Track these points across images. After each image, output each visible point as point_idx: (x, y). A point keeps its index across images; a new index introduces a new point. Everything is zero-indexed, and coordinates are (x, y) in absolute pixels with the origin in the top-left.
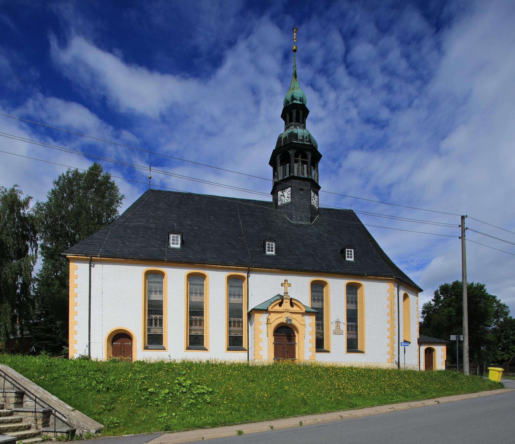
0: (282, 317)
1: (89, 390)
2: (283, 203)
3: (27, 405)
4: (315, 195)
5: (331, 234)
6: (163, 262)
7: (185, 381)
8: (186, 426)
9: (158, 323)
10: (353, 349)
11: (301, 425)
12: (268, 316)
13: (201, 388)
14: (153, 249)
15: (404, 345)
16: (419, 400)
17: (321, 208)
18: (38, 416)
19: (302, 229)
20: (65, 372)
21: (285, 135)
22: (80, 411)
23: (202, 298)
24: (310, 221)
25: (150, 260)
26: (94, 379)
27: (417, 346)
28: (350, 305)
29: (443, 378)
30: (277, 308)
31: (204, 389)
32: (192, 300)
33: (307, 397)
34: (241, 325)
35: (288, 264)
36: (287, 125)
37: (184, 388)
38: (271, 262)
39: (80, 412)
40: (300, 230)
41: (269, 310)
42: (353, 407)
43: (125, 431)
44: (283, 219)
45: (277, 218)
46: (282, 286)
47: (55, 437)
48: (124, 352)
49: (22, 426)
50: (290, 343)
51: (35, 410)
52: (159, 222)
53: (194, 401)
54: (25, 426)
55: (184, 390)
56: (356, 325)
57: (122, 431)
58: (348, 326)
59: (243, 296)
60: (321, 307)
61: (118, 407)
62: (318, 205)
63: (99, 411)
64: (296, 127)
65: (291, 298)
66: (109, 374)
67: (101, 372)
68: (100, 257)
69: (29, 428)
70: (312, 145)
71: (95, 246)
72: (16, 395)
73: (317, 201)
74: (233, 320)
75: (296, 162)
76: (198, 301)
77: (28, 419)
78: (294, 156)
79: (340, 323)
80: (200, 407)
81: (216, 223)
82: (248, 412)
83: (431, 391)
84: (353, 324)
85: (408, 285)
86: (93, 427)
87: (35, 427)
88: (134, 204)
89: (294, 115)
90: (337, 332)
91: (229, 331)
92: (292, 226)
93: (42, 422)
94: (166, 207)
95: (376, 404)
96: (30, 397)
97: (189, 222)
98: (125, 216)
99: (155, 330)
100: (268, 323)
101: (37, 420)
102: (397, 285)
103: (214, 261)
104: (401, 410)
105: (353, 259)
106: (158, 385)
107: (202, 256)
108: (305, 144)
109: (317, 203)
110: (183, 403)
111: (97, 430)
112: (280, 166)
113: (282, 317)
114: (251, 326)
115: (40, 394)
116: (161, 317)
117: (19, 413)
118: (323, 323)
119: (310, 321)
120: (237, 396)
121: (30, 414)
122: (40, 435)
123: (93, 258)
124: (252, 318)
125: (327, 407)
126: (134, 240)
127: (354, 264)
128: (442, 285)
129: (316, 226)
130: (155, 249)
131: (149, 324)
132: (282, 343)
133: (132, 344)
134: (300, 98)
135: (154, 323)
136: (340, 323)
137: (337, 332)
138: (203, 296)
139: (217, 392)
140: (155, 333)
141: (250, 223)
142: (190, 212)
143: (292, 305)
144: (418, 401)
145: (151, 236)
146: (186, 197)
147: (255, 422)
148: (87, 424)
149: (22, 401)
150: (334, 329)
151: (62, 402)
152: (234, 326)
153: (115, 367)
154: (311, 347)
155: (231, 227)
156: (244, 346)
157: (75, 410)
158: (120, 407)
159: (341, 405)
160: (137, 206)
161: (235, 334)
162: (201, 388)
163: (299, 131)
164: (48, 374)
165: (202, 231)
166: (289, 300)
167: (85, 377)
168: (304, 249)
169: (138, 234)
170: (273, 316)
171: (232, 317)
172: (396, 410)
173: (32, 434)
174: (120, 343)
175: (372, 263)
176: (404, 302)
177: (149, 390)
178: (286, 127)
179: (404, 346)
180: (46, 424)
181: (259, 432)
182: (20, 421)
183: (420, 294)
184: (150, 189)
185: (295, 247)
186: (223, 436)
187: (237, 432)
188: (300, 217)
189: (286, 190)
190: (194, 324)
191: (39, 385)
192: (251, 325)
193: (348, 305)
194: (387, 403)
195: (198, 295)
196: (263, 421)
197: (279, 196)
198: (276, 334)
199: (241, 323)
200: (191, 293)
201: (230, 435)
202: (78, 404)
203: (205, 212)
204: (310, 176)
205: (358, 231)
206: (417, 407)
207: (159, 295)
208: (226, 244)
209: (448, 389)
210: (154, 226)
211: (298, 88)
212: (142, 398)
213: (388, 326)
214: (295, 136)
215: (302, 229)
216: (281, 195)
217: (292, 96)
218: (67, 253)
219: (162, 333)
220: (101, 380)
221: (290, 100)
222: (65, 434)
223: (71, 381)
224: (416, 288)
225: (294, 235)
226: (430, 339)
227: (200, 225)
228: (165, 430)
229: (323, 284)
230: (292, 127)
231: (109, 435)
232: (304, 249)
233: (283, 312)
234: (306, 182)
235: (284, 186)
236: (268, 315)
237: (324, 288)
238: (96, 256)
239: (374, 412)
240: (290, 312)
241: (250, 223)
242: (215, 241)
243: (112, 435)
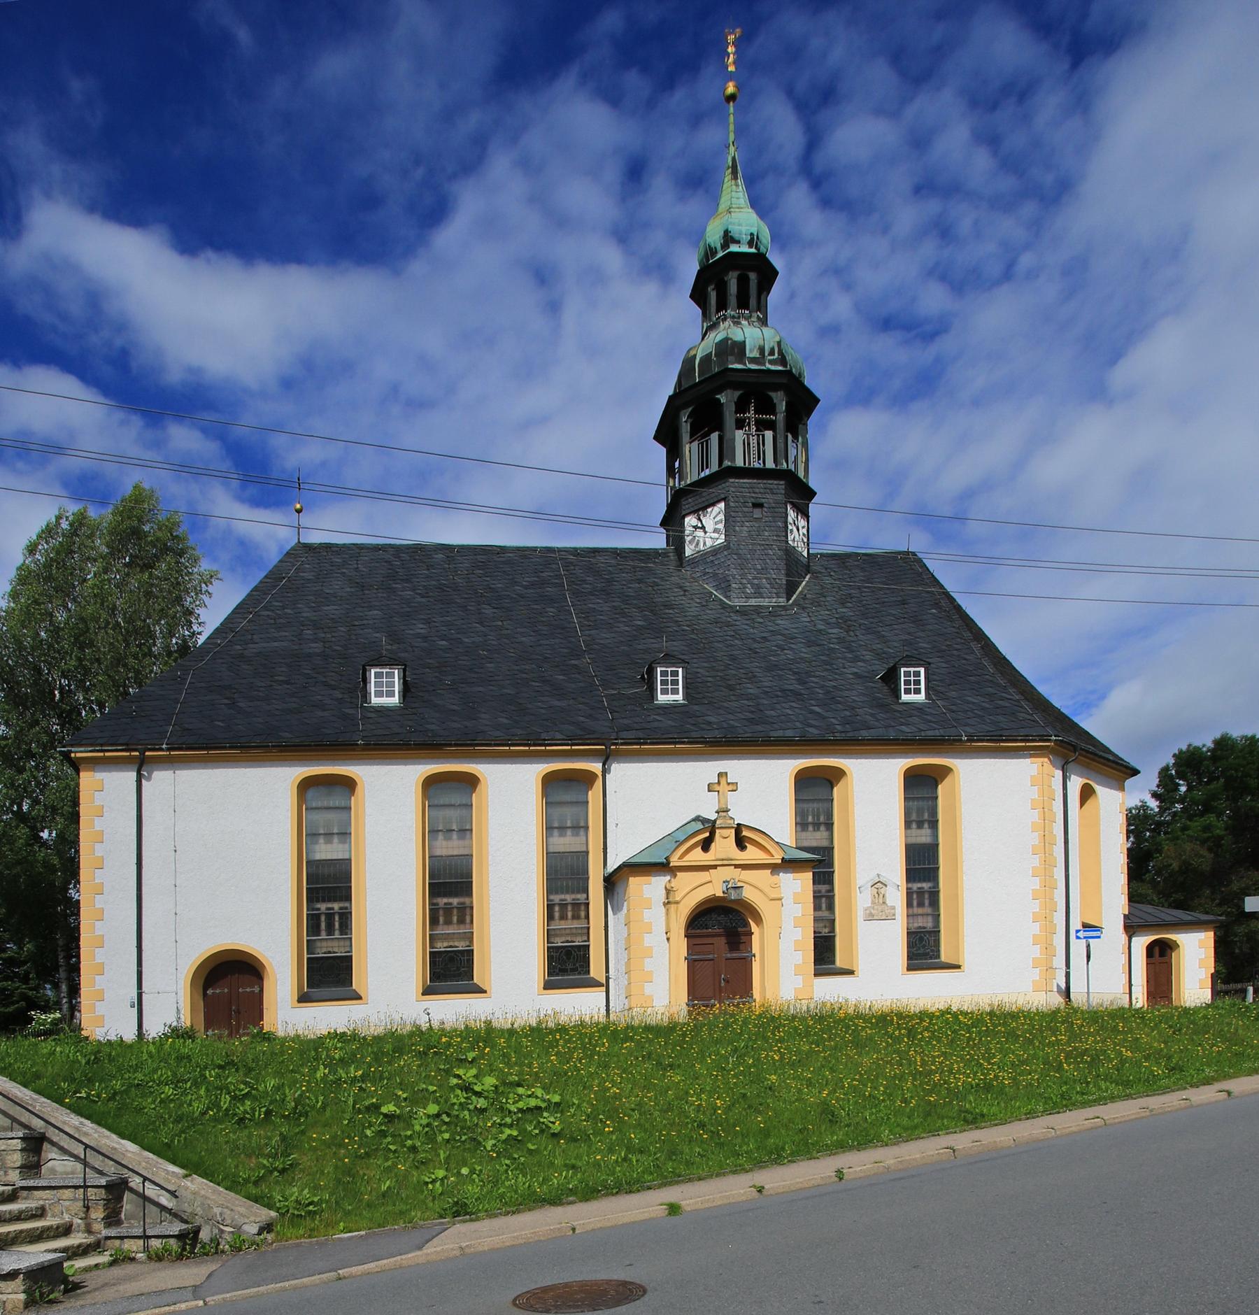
0: (711, 882)
1: (216, 1120)
2: (702, 548)
3: (53, 1171)
4: (799, 518)
5: (852, 629)
6: (354, 750)
7: (477, 1079)
8: (511, 1201)
9: (337, 925)
10: (926, 959)
11: (841, 1179)
12: (669, 881)
13: (529, 1096)
14: (320, 713)
15: (1085, 938)
16: (1165, 1090)
17: (816, 555)
18: (93, 1198)
19: (761, 620)
20: (140, 1076)
21: (703, 349)
22: (203, 1178)
23: (467, 842)
24: (784, 595)
25: (315, 745)
26: (224, 1088)
27: (1123, 938)
28: (914, 831)
29: (1229, 1024)
30: (698, 856)
31: (537, 1097)
32: (438, 852)
33: (838, 1100)
34: (583, 914)
35: (725, 725)
36: (710, 320)
37: (479, 1097)
38: (673, 724)
39: (205, 1181)
40: (756, 625)
41: (671, 864)
42: (975, 1123)
43: (342, 1224)
44: (702, 596)
45: (682, 593)
46: (709, 791)
47: (144, 1252)
48: (239, 1013)
49: (52, 1226)
50: (735, 955)
51: (85, 1181)
52: (333, 637)
53: (515, 1133)
54: (58, 1227)
55: (482, 1103)
56: (934, 888)
57: (331, 1225)
58: (909, 893)
59: (590, 829)
60: (825, 843)
61: (306, 1161)
62: (808, 545)
63: (256, 1174)
64: (737, 323)
65: (738, 824)
66: (260, 1073)
67: (237, 1070)
68: (168, 749)
69: (66, 1230)
70: (790, 372)
71: (152, 721)
72: (24, 1146)
73: (804, 534)
74: (561, 900)
75: (740, 424)
76: (455, 853)
77: (65, 1209)
78: (734, 409)
79: (886, 886)
80: (533, 1148)
81: (500, 623)
82: (674, 1153)
83: (1197, 1064)
84: (926, 886)
85: (1097, 758)
86: (252, 1219)
87: (83, 1226)
88: (255, 589)
89: (733, 287)
90: (879, 913)
91: (550, 933)
92: (731, 614)
93: (104, 1212)
94: (348, 589)
95: (1041, 1109)
96: (63, 1150)
97: (421, 628)
98: (231, 626)
99: (329, 946)
100: (669, 903)
101: (88, 1208)
102: (1060, 762)
103: (502, 734)
104: (1120, 1122)
105: (921, 697)
106: (405, 1095)
107: (465, 723)
108: (769, 371)
109: (805, 540)
110: (484, 1140)
111: (261, 1224)
112: (691, 443)
113: (711, 882)
114: (614, 914)
115: (90, 1137)
116: (346, 908)
117: (36, 1192)
118: (832, 890)
119: (799, 885)
120: (633, 1110)
121: (68, 1193)
122: (99, 1248)
123: (147, 753)
124: (619, 889)
125: (898, 1125)
126: (261, 694)
127: (927, 709)
128: (1181, 752)
129: (804, 608)
130: (326, 714)
131: (310, 930)
132: (711, 956)
133: (262, 990)
134: (749, 238)
135: (323, 925)
136: (886, 886)
137: (879, 913)
138: (468, 836)
139: (574, 1104)
140: (330, 952)
141: (601, 617)
142: (423, 600)
143: (741, 843)
144: (1164, 1093)
145: (313, 678)
146: (408, 558)
147: (700, 1179)
148: (232, 1210)
149: (39, 1161)
150: (865, 906)
151: (151, 1155)
152: (563, 917)
153: (273, 1053)
154: (801, 962)
155: (545, 633)
156: (592, 974)
157: (190, 1175)
158: (311, 1159)
159: (938, 1118)
160: (265, 594)
161: (568, 942)
162: (529, 1096)
163: (750, 334)
164: (97, 1084)
165: (459, 650)
166: (733, 831)
167: (196, 1084)
168: (771, 679)
169: (272, 677)
170: (684, 882)
171: (557, 893)
172: (1107, 1122)
173: (79, 1246)
174: (226, 990)
175: (984, 704)
176: (1081, 807)
177: (384, 1110)
178: (705, 325)
179: (1085, 940)
180: (112, 1218)
181: (725, 1205)
182: (40, 1213)
183: (1129, 782)
184: (299, 542)
185: (743, 676)
186: (626, 1220)
187: (665, 1207)
188: (752, 585)
189: (709, 510)
190: (441, 919)
191: (82, 1115)
192: (616, 910)
193: (909, 831)
194: (1074, 1105)
195: (455, 836)
196: (724, 1174)
197: (688, 530)
198: (693, 931)
199: (583, 907)
200: (434, 832)
201: (646, 1216)
202: (195, 1158)
203: (466, 596)
204: (785, 464)
205: (934, 611)
206: (1169, 1112)
207: (341, 846)
208: (533, 683)
209: (1249, 1055)
210: (316, 647)
211: (742, 206)
212: (368, 1132)
213: (1036, 883)
214: (736, 350)
215: (761, 620)
216: (696, 527)
217: (726, 233)
218: (72, 746)
219: (349, 952)
220: (243, 1090)
222: (172, 1241)
223: (161, 1099)
224: (1119, 767)
225: (737, 639)
226: (1163, 916)
227: (452, 634)
228: (454, 1213)
229: (832, 777)
230: (727, 323)
231: (297, 1238)
232: (771, 679)
233: (715, 867)
234: (770, 482)
235: (703, 499)
236: (668, 878)
237: (835, 789)
238: (157, 747)
239: (1045, 1130)
240: (736, 866)
241: (601, 617)
242: (500, 678)
243: (306, 1238)
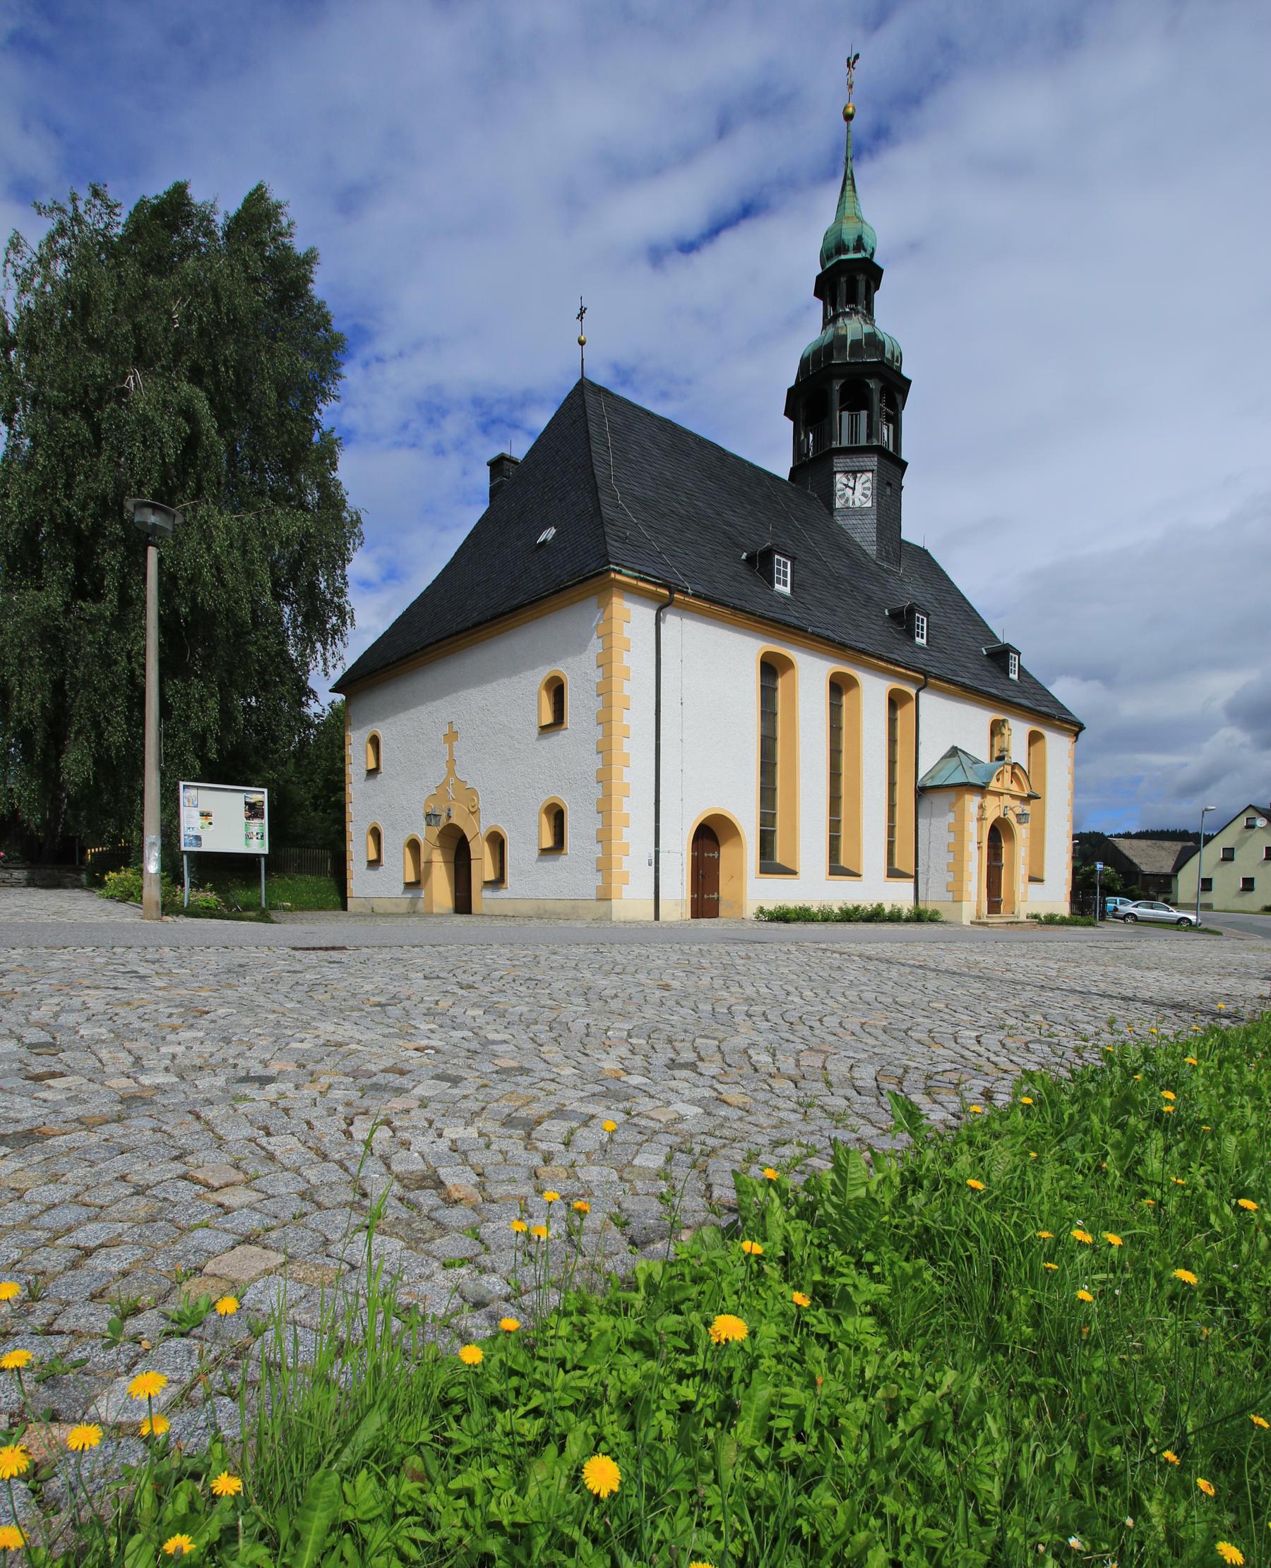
170: (991, 801)
197: (839, 486)
221: (851, 246)
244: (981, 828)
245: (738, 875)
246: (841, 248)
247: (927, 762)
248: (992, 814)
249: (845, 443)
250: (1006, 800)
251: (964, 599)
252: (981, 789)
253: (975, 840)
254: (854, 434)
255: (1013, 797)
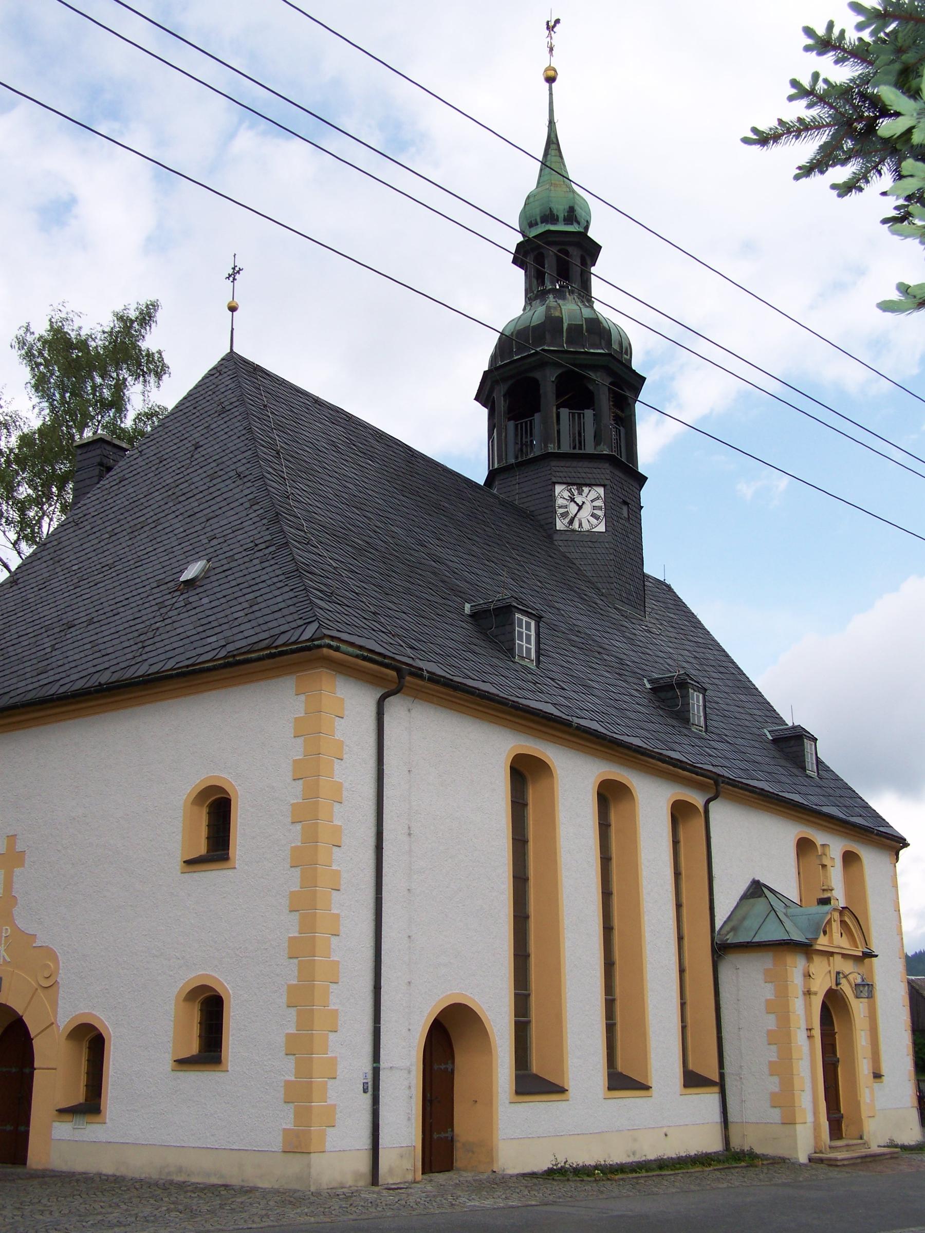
197: (560, 501)
221: (561, 217)
244: (808, 1007)
245: (487, 1099)
246: (549, 217)
247: (724, 908)
248: (821, 985)
249: (566, 448)
250: (839, 964)
251: (727, 656)
252: (806, 949)
253: (803, 1026)
254: (579, 441)
255: (844, 956)
